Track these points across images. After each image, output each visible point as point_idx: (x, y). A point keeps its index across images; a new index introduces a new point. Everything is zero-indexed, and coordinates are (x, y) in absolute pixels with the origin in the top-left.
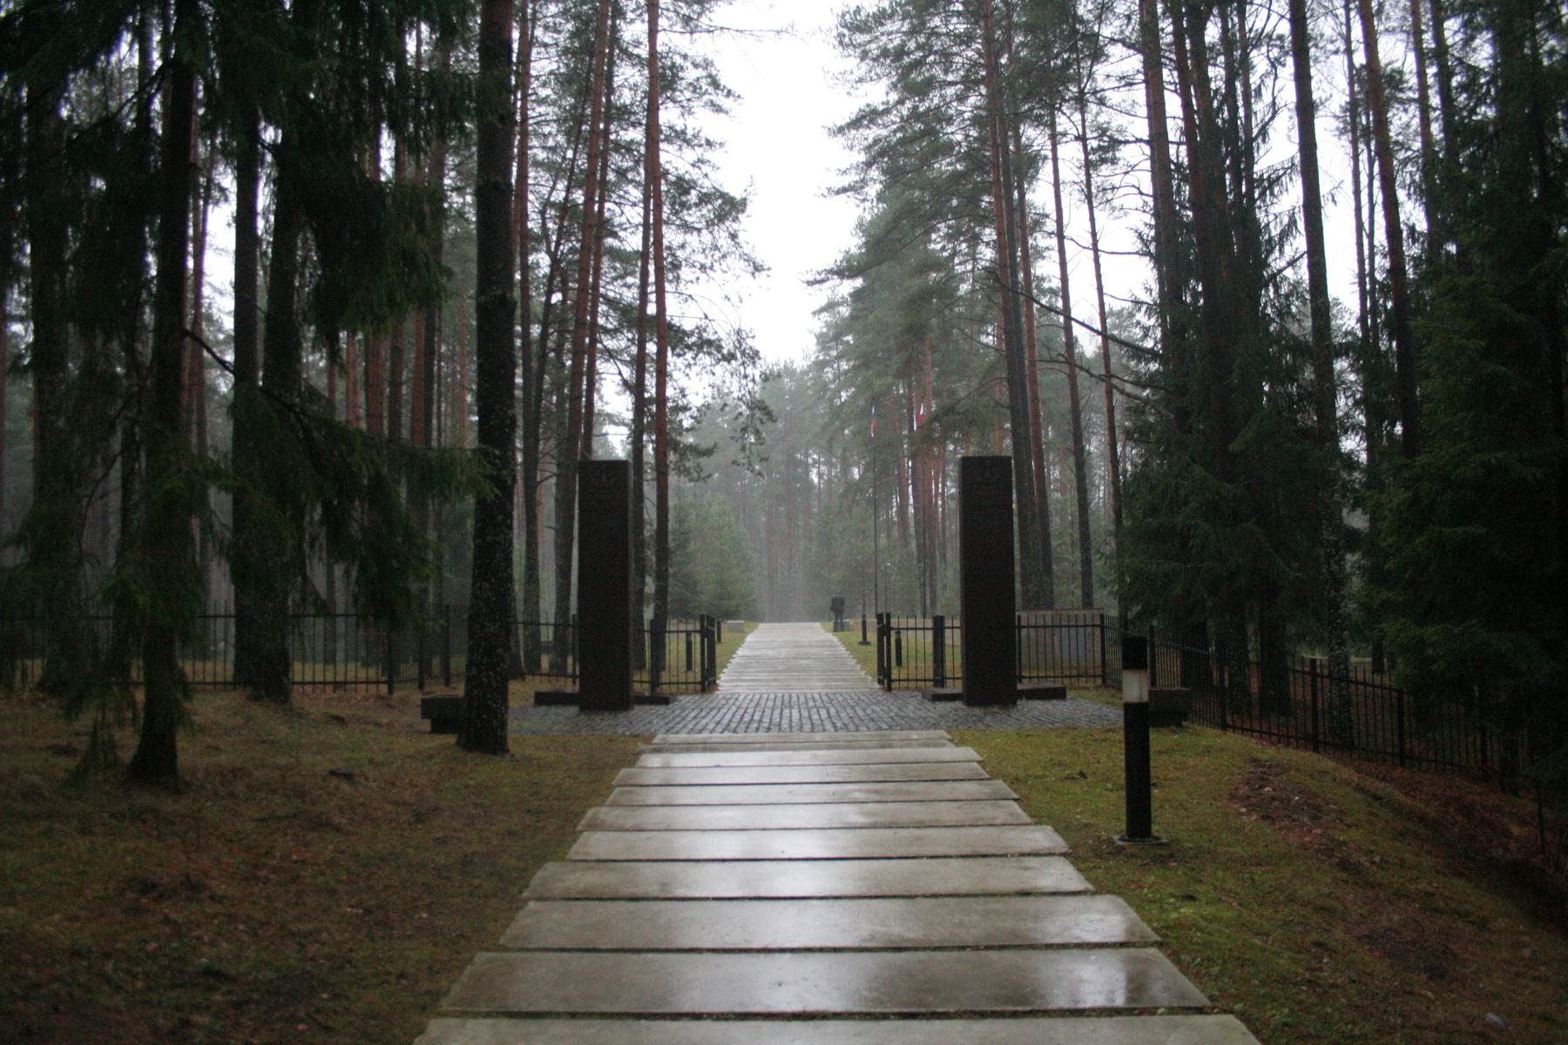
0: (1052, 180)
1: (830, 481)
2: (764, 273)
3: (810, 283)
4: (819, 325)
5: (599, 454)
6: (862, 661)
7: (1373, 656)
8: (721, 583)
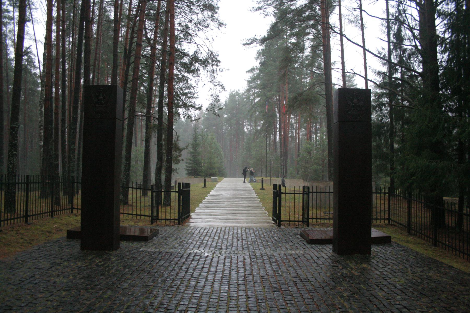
0: (338, 14)
1: (250, 131)
2: (223, 26)
3: (244, 45)
4: (249, 76)
7: (460, 198)
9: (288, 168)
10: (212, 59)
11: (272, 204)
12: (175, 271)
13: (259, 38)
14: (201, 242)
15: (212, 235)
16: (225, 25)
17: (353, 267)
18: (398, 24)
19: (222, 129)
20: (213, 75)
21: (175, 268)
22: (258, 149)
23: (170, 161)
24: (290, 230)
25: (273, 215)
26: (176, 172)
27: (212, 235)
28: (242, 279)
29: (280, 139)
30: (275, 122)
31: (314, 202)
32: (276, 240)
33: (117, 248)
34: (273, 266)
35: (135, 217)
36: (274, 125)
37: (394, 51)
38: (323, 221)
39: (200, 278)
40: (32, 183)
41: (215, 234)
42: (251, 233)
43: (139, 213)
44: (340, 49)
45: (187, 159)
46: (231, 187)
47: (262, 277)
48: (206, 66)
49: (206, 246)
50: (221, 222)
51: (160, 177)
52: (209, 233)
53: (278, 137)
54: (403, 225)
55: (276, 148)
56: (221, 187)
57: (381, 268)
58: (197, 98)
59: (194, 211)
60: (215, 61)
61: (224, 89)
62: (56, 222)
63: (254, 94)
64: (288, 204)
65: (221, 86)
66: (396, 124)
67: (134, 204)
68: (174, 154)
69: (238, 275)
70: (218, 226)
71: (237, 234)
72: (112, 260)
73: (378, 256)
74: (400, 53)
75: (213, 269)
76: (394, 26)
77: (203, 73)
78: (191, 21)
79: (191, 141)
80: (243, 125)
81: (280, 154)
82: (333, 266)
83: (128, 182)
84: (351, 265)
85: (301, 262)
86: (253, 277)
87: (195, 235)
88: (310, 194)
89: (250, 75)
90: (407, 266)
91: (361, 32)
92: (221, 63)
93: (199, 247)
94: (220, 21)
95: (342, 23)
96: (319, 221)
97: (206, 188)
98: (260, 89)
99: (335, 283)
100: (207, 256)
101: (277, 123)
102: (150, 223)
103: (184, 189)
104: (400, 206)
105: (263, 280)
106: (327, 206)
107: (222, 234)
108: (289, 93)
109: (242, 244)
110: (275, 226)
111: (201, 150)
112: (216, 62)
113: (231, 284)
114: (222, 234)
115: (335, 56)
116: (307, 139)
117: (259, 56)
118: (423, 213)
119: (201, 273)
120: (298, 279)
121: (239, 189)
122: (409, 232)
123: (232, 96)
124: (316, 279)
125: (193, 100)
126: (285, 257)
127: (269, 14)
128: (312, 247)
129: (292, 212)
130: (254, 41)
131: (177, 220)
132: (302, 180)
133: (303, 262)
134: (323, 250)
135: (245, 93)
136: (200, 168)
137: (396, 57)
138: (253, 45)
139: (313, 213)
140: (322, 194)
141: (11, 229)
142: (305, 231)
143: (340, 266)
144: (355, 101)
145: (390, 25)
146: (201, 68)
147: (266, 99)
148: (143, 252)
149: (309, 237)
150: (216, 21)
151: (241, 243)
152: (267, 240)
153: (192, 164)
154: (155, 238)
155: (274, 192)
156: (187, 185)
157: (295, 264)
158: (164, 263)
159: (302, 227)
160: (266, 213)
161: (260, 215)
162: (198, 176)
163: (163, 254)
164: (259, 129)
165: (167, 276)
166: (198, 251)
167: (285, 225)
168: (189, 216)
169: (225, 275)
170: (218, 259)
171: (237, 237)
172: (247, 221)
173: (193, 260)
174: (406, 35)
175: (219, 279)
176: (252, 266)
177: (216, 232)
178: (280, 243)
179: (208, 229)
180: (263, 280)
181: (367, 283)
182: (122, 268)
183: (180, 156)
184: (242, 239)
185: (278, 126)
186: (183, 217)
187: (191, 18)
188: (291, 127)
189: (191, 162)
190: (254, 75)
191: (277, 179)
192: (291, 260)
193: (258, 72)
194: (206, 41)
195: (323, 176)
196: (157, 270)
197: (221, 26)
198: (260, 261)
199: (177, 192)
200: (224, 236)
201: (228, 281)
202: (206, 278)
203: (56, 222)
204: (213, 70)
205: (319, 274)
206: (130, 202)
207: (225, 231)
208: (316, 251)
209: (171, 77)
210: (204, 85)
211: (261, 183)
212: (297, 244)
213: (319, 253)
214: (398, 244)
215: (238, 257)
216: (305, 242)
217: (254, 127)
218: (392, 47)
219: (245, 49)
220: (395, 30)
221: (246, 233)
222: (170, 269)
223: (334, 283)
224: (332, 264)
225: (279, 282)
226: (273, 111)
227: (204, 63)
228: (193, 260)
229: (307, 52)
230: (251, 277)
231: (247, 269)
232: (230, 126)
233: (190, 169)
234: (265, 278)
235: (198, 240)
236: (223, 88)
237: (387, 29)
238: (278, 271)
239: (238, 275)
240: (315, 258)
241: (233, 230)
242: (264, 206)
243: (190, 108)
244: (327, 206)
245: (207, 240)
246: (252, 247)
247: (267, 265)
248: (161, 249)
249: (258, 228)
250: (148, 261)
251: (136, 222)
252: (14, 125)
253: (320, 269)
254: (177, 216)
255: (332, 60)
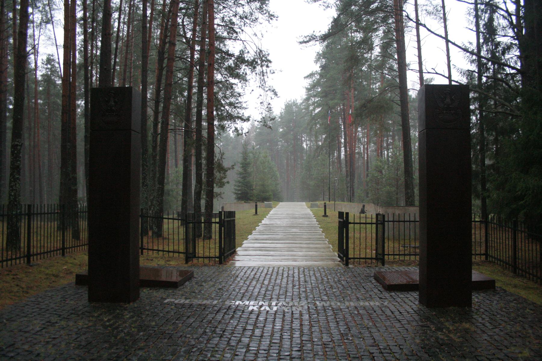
1: (310, 147)
2: (274, 19)
3: (301, 43)
4: (308, 82)
5: (115, 86)
6: (326, 230)
8: (263, 185)
9: (355, 190)
10: (262, 59)
11: (337, 235)
12: (206, 335)
13: (318, 34)
14: (246, 288)
15: (261, 279)
16: (277, 17)
17: (451, 328)
18: (489, 12)
19: (277, 145)
20: (263, 78)
21: (207, 331)
22: (319, 168)
23: (210, 184)
24: (361, 270)
25: (339, 251)
26: (221, 197)
27: (261, 279)
28: (297, 349)
29: (346, 156)
30: (338, 136)
31: (391, 233)
32: (343, 286)
33: (136, 297)
34: (340, 327)
35: (166, 255)
36: (338, 140)
37: (484, 46)
38: (402, 258)
39: (239, 347)
40: (46, 213)
41: (265, 278)
42: (311, 275)
43: (171, 249)
44: (417, 47)
45: (236, 182)
46: (287, 214)
47: (325, 345)
48: (255, 68)
49: (251, 295)
50: (274, 260)
51: (200, 204)
52: (257, 276)
53: (343, 153)
54: (503, 261)
55: (340, 166)
56: (275, 214)
57: (490, 329)
58: (246, 108)
59: (241, 245)
60: (264, 60)
61: (277, 95)
62: (67, 262)
63: (314, 103)
64: (357, 235)
65: (273, 91)
66: (488, 135)
67: (171, 237)
68: (217, 175)
69: (291, 342)
70: (269, 265)
71: (294, 277)
72: (125, 317)
73: (482, 310)
74: (492, 47)
75: (258, 332)
76: (484, 14)
77: (251, 76)
78: (235, 16)
79: (240, 160)
80: (302, 140)
81: (345, 173)
82: (422, 326)
83: (161, 211)
84: (447, 324)
85: (379, 320)
86: (313, 345)
87: (239, 279)
88: (386, 223)
89: (309, 81)
90: (526, 326)
91: (443, 25)
92: (272, 63)
93: (242, 297)
94: (271, 13)
95: (419, 15)
96: (397, 257)
97: (258, 216)
98: (321, 97)
99: (430, 356)
100: (253, 310)
101: (341, 137)
102: (185, 262)
103: (226, 219)
104: (496, 236)
105: (327, 350)
106: (407, 237)
107: (273, 277)
108: (356, 101)
109: (299, 292)
110: (341, 264)
111: (252, 170)
112: (266, 62)
113: (281, 357)
114: (273, 277)
115: (411, 56)
116: (378, 156)
117: (319, 58)
118: (527, 245)
119: (241, 337)
120: (376, 348)
121: (297, 216)
122: (515, 272)
123: (289, 107)
124: (400, 349)
125: (241, 111)
126: (356, 312)
127: (329, 5)
128: (391, 296)
129: (363, 246)
130: (312, 38)
131: (217, 258)
132: (373, 205)
133: (381, 320)
134: (406, 300)
135: (303, 103)
136: (252, 192)
137: (486, 53)
138: (311, 43)
139: (389, 246)
140: (401, 223)
141: (7, 273)
142: (380, 273)
143: (432, 326)
144: (448, 100)
145: (480, 13)
146: (248, 71)
147: (328, 108)
148: (168, 304)
149: (385, 280)
150: (266, 13)
151: (298, 290)
152: (331, 285)
153: (242, 186)
154: (187, 283)
155: (340, 222)
156: (231, 214)
157: (371, 324)
158: (194, 321)
159: (376, 266)
160: (329, 247)
161: (322, 250)
162: (249, 201)
163: (193, 307)
164: (320, 144)
165: (194, 343)
166: (241, 303)
167: (354, 263)
168: (234, 253)
169: (274, 341)
170: (266, 315)
171: (293, 281)
172: (306, 258)
173: (232, 317)
174: (500, 25)
175: (265, 348)
176: (311, 326)
177: (267, 274)
178: (348, 290)
179: (256, 270)
180: (327, 350)
181: (475, 356)
182: (136, 330)
183: (225, 178)
184: (299, 285)
185: (343, 141)
186: (225, 255)
187: (236, 11)
188: (358, 141)
189: (240, 184)
190: (313, 81)
191: (342, 203)
192: (364, 317)
193: (318, 77)
194: (254, 38)
195: (397, 198)
196: (181, 334)
197: (271, 19)
198: (322, 318)
199: (217, 223)
200: (275, 280)
201: (277, 351)
202: (248, 346)
203: (67, 262)
204: (263, 71)
205: (405, 340)
206: (165, 234)
207: (278, 273)
208: (397, 302)
209: (211, 80)
210: (253, 90)
211: (323, 208)
212: (370, 291)
213: (402, 306)
214: (505, 291)
215: (292, 312)
216: (382, 289)
217: (314, 143)
218: (481, 41)
219: (302, 48)
220: (486, 19)
221: (305, 276)
222: (201, 331)
223: (426, 356)
224: (420, 323)
225: (349, 354)
226: (336, 123)
227: (252, 64)
228: (232, 317)
229: (377, 51)
230: (309, 345)
231: (305, 331)
232: (287, 141)
233: (239, 192)
234: (330, 346)
235: (242, 286)
236: (276, 94)
237: (475, 19)
238: (347, 335)
239: (291, 342)
240: (397, 313)
241: (288, 271)
242: (327, 238)
243: (237, 120)
244: (407, 237)
245: (254, 285)
246: (311, 296)
247: (332, 325)
248: (192, 300)
249: (319, 268)
250: (173, 319)
251: (168, 261)
252: (16, 143)
253: (406, 331)
254: (218, 252)
255: (407, 61)
